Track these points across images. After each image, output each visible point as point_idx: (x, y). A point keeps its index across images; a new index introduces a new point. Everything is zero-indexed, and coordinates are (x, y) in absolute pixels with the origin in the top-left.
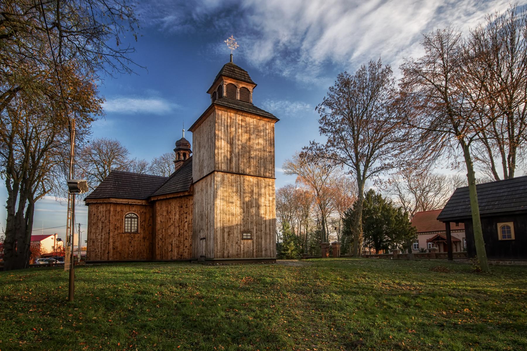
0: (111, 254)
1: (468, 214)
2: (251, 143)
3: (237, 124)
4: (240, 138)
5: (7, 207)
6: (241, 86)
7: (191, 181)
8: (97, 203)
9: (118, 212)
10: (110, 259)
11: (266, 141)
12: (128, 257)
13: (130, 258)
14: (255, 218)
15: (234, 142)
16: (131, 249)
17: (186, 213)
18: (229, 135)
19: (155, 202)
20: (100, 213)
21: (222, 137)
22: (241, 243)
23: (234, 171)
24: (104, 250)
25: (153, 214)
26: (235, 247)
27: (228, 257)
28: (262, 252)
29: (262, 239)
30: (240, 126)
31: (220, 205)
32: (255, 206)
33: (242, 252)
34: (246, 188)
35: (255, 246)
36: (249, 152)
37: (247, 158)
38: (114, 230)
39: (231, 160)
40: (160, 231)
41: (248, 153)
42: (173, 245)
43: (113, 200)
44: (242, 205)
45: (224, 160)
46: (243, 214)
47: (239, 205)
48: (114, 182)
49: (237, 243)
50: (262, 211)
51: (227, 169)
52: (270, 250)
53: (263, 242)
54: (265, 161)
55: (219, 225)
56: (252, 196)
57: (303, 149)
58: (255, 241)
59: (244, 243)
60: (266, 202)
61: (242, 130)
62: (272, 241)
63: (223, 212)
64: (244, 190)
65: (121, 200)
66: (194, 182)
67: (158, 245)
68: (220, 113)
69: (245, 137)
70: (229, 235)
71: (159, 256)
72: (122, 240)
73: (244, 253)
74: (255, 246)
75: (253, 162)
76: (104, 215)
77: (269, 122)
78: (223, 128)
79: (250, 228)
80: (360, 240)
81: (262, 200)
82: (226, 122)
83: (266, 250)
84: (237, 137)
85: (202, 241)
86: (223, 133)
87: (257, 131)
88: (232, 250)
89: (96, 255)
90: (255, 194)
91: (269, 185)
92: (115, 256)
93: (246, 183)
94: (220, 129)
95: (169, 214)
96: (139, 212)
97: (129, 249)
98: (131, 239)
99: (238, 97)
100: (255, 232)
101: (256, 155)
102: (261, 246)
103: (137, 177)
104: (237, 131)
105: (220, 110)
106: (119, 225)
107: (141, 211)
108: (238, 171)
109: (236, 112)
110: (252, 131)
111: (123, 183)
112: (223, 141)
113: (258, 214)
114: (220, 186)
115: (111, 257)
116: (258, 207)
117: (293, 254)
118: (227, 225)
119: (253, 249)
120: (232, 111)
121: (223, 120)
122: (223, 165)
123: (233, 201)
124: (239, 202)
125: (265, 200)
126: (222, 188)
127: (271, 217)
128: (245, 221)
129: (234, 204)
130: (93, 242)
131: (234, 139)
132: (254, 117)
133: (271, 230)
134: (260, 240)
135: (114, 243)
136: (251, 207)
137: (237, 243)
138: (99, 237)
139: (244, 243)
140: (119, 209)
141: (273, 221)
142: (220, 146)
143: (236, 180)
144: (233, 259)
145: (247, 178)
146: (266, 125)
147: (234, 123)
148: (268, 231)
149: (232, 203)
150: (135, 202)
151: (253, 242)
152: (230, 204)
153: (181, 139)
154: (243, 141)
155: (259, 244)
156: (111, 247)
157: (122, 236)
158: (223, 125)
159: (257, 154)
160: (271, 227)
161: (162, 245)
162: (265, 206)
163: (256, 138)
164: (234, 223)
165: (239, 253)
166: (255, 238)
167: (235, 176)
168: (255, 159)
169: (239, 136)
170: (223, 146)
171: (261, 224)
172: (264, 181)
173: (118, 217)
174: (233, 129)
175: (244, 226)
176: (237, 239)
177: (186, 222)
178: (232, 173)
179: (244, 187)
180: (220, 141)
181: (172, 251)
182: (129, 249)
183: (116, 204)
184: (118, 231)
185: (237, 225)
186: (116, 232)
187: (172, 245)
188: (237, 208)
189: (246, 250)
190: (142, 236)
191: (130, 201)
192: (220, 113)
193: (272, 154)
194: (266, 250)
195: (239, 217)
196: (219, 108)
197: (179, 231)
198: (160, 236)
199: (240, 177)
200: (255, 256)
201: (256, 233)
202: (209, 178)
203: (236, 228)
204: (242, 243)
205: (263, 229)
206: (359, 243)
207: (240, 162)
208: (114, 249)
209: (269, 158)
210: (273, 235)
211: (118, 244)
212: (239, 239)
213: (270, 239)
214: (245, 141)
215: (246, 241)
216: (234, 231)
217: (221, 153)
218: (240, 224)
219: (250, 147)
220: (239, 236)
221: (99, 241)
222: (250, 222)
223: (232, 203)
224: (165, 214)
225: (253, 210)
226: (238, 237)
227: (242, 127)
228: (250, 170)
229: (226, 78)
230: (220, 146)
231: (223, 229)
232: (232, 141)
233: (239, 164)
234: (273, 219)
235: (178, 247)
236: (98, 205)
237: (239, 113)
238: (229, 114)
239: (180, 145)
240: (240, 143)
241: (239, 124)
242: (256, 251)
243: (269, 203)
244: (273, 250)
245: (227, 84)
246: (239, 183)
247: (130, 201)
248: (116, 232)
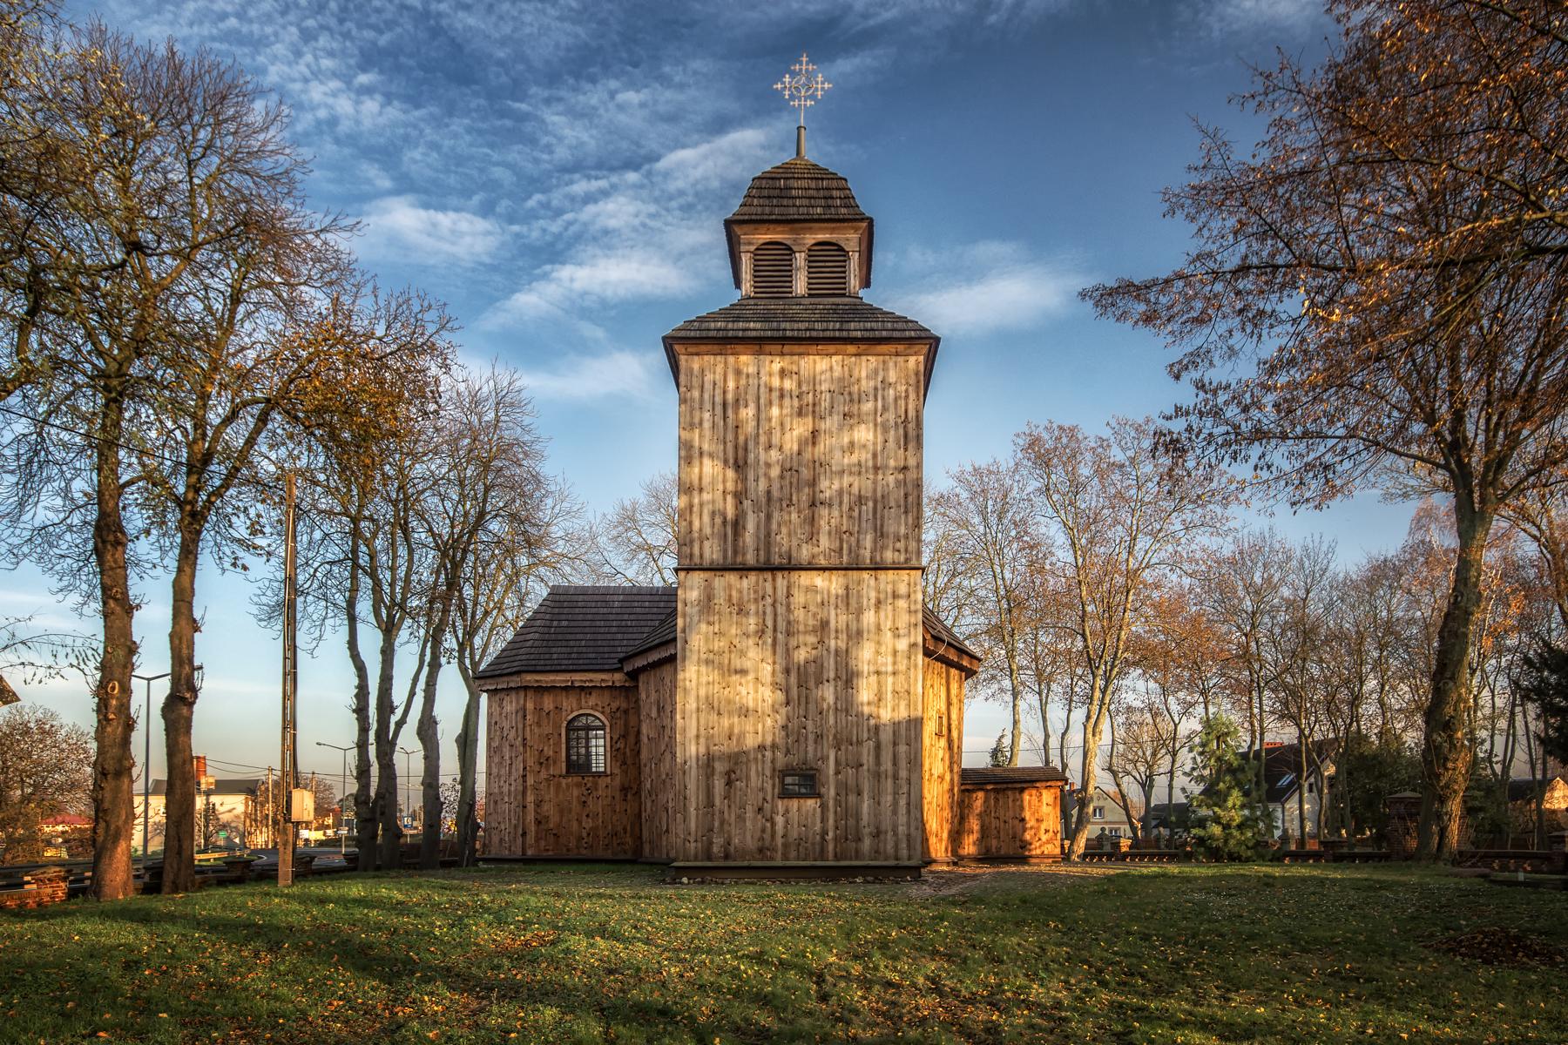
0: (531, 839)
2: (820, 448)
3: (762, 389)
4: (775, 440)
5: (354, 711)
6: (810, 239)
9: (548, 714)
10: (530, 853)
11: (885, 430)
12: (578, 848)
13: (584, 852)
14: (832, 721)
15: (751, 456)
16: (588, 824)
18: (730, 436)
21: (706, 447)
22: (774, 811)
23: (750, 559)
26: (752, 822)
27: (727, 857)
28: (859, 840)
29: (859, 794)
30: (775, 395)
31: (698, 684)
32: (832, 675)
33: (779, 841)
34: (799, 614)
35: (831, 821)
36: (813, 483)
37: (804, 505)
38: (537, 768)
39: (738, 525)
41: (806, 490)
43: (530, 679)
44: (780, 678)
45: (713, 525)
46: (783, 711)
47: (768, 679)
48: (548, 623)
49: (760, 810)
50: (865, 693)
51: (725, 557)
52: (895, 834)
53: (865, 805)
54: (879, 506)
55: (692, 749)
56: (821, 642)
57: (1169, 418)
58: (831, 803)
59: (787, 811)
60: (880, 660)
61: (781, 407)
62: (903, 802)
63: (711, 705)
64: (789, 623)
65: (552, 677)
68: (696, 363)
69: (801, 428)
70: (729, 783)
72: (561, 796)
73: (785, 845)
74: (831, 821)
75: (828, 519)
77: (897, 355)
78: (707, 416)
79: (810, 755)
80: (1447, 786)
81: (865, 655)
82: (718, 391)
83: (877, 834)
84: (763, 439)
86: (707, 433)
87: (848, 402)
88: (745, 835)
90: (833, 635)
91: (895, 596)
92: (543, 843)
93: (799, 598)
94: (696, 420)
96: (607, 710)
97: (580, 822)
98: (586, 793)
99: (800, 285)
100: (831, 771)
101: (840, 492)
103: (621, 598)
104: (763, 416)
105: (697, 354)
106: (551, 753)
107: (615, 705)
108: (768, 559)
109: (757, 347)
110: (825, 404)
111: (572, 624)
112: (707, 462)
113: (846, 705)
114: (696, 619)
115: (531, 846)
116: (848, 678)
117: (1232, 842)
118: (724, 749)
119: (824, 832)
120: (739, 348)
121: (708, 386)
122: (707, 544)
123: (748, 664)
124: (769, 668)
125: (878, 653)
126: (703, 627)
127: (903, 713)
128: (792, 732)
129: (751, 677)
131: (751, 445)
132: (832, 348)
133: (903, 763)
134: (852, 798)
135: (538, 804)
136: (819, 682)
137: (760, 810)
139: (787, 811)
140: (548, 703)
141: (908, 729)
142: (696, 482)
143: (756, 592)
144: (746, 863)
145: (805, 578)
146: (885, 369)
147: (752, 391)
148: (887, 765)
149: (743, 672)
150: (591, 681)
151: (824, 807)
152: (735, 678)
154: (787, 447)
155: (848, 814)
156: (531, 817)
157: (559, 785)
158: (708, 406)
159: (845, 484)
160: (902, 748)
162: (878, 673)
163: (840, 428)
164: (751, 742)
165: (767, 843)
166: (832, 792)
167: (753, 577)
168: (836, 507)
169: (770, 433)
170: (706, 481)
171: (859, 743)
172: (872, 582)
173: (548, 729)
174: (748, 413)
175: (788, 752)
176: (761, 795)
178: (743, 570)
179: (789, 610)
180: (696, 462)
181: (667, 831)
182: (580, 822)
183: (540, 690)
184: (548, 769)
185: (761, 748)
188: (761, 689)
189: (794, 834)
190: (617, 781)
191: (578, 678)
192: (696, 366)
193: (912, 475)
194: (877, 834)
195: (769, 722)
196: (691, 349)
199: (774, 580)
200: (831, 855)
201: (837, 773)
203: (756, 759)
204: (781, 808)
205: (867, 758)
206: (1443, 800)
207: (774, 526)
208: (538, 822)
209: (896, 495)
211: (549, 809)
212: (769, 798)
213: (895, 793)
214: (795, 448)
215: (794, 804)
216: (748, 769)
217: (701, 505)
218: (774, 746)
219: (818, 465)
220: (768, 787)
222: (811, 737)
223: (743, 672)
225: (828, 693)
226: (762, 789)
227: (782, 396)
228: (816, 550)
229: (746, 228)
230: (696, 482)
231: (708, 762)
232: (741, 452)
233: (768, 535)
234: (909, 721)
236: (502, 695)
237: (767, 348)
238: (731, 359)
240: (774, 455)
241: (771, 390)
242: (836, 839)
243: (894, 663)
244: (909, 835)
245: (752, 248)
246: (769, 600)
247: (577, 677)
248: (543, 775)
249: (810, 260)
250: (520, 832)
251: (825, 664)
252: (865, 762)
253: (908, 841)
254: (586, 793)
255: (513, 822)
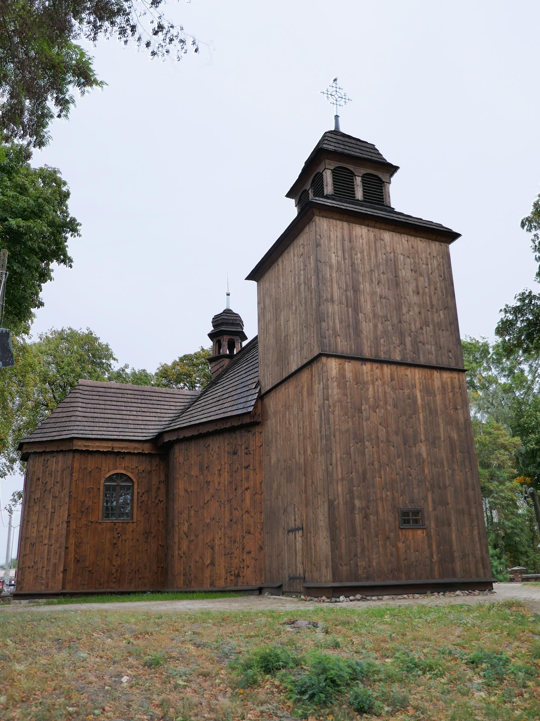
1: (180, 581)
7: (257, 390)
8: (44, 452)
16: (117, 562)
17: (247, 467)
19: (171, 444)
20: (50, 474)
24: (55, 564)
25: (167, 476)
28: (453, 561)
32: (423, 437)
35: (434, 547)
40: (185, 515)
42: (217, 548)
66: (263, 392)
67: (179, 549)
70: (366, 517)
71: (182, 578)
74: (434, 547)
76: (59, 480)
83: (464, 556)
85: (291, 536)
89: (36, 578)
95: (206, 472)
97: (111, 561)
102: (451, 546)
106: (91, 503)
107: (141, 468)
130: (33, 545)
138: (46, 533)
150: (127, 448)
151: (429, 535)
153: (224, 312)
156: (71, 556)
161: (189, 548)
166: (433, 525)
171: (445, 487)
177: (247, 489)
181: (212, 563)
182: (111, 561)
186: (83, 521)
187: (213, 548)
197: (231, 514)
198: (185, 528)
200: (436, 574)
202: (305, 375)
210: (477, 515)
221: (46, 541)
224: (195, 472)
235: (229, 554)
236: (48, 457)
239: (222, 324)
248: (83, 521)
249: (363, 182)
250: (61, 568)
251: (419, 430)
252: (449, 501)
253: (482, 561)
254: (116, 536)
255: (53, 561)
